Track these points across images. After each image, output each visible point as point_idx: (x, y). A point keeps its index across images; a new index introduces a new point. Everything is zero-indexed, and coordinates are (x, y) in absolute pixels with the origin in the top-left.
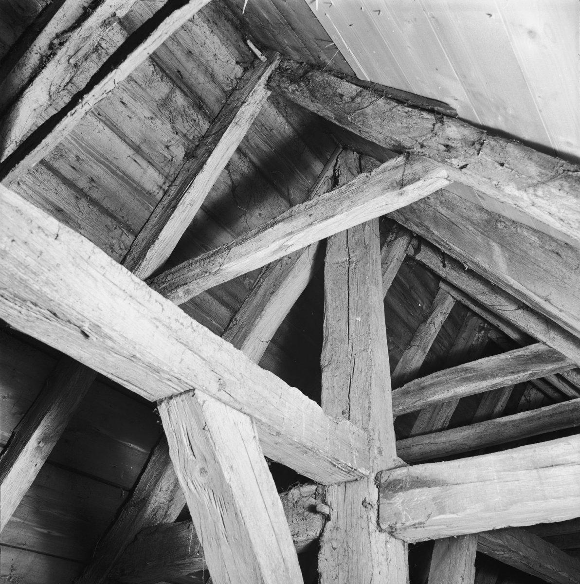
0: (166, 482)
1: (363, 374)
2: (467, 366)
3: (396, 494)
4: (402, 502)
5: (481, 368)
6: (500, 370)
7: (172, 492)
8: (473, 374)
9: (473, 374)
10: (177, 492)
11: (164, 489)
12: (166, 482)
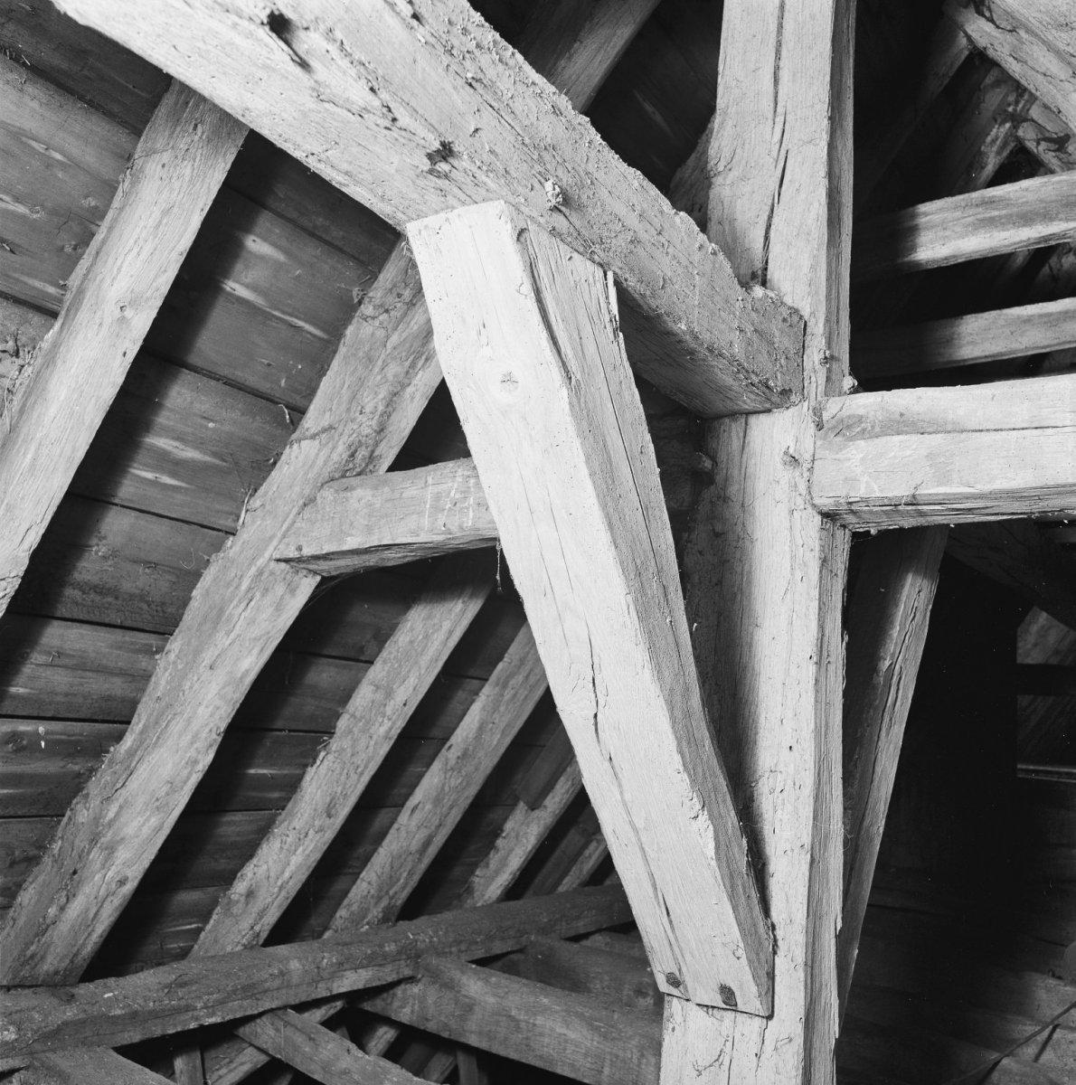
0: (371, 397)
1: (803, 196)
2: (994, 193)
3: (851, 443)
4: (862, 459)
5: (1024, 200)
6: (1067, 205)
7: (382, 415)
8: (1004, 212)
9: (1004, 212)
10: (392, 418)
11: (368, 409)
12: (371, 397)
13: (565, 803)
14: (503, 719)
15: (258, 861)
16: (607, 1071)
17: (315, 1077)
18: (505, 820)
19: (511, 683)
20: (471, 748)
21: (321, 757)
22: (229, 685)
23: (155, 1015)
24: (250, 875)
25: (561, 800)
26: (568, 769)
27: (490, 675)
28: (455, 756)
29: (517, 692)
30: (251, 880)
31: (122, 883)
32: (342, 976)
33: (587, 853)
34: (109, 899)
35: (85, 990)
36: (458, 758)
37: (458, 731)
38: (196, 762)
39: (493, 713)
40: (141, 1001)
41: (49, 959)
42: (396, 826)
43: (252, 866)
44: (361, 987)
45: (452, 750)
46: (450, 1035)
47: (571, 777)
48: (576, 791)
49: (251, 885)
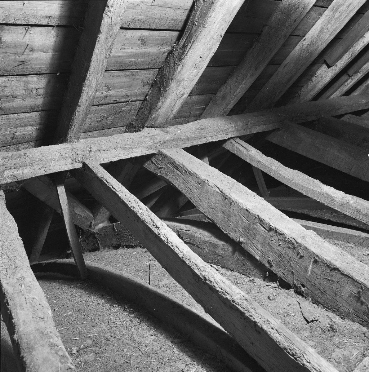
13: (346, 64)
14: (333, 27)
15: (227, 85)
16: (353, 169)
17: (247, 161)
18: (317, 70)
19: (340, 9)
20: (315, 40)
21: (255, 45)
22: (227, 14)
23: (195, 138)
24: (223, 90)
25: (345, 62)
26: (351, 49)
27: (329, 6)
28: (307, 44)
29: (341, 15)
30: (224, 92)
31: (183, 95)
32: (255, 127)
33: (346, 83)
34: (179, 100)
35: (171, 129)
36: (308, 44)
37: (310, 32)
38: (211, 49)
39: (328, 24)
40: (189, 134)
41: (159, 119)
42: (277, 72)
43: (224, 87)
44: (261, 131)
45: (305, 41)
46: (291, 149)
47: (352, 53)
48: (352, 59)
49: (224, 94)
